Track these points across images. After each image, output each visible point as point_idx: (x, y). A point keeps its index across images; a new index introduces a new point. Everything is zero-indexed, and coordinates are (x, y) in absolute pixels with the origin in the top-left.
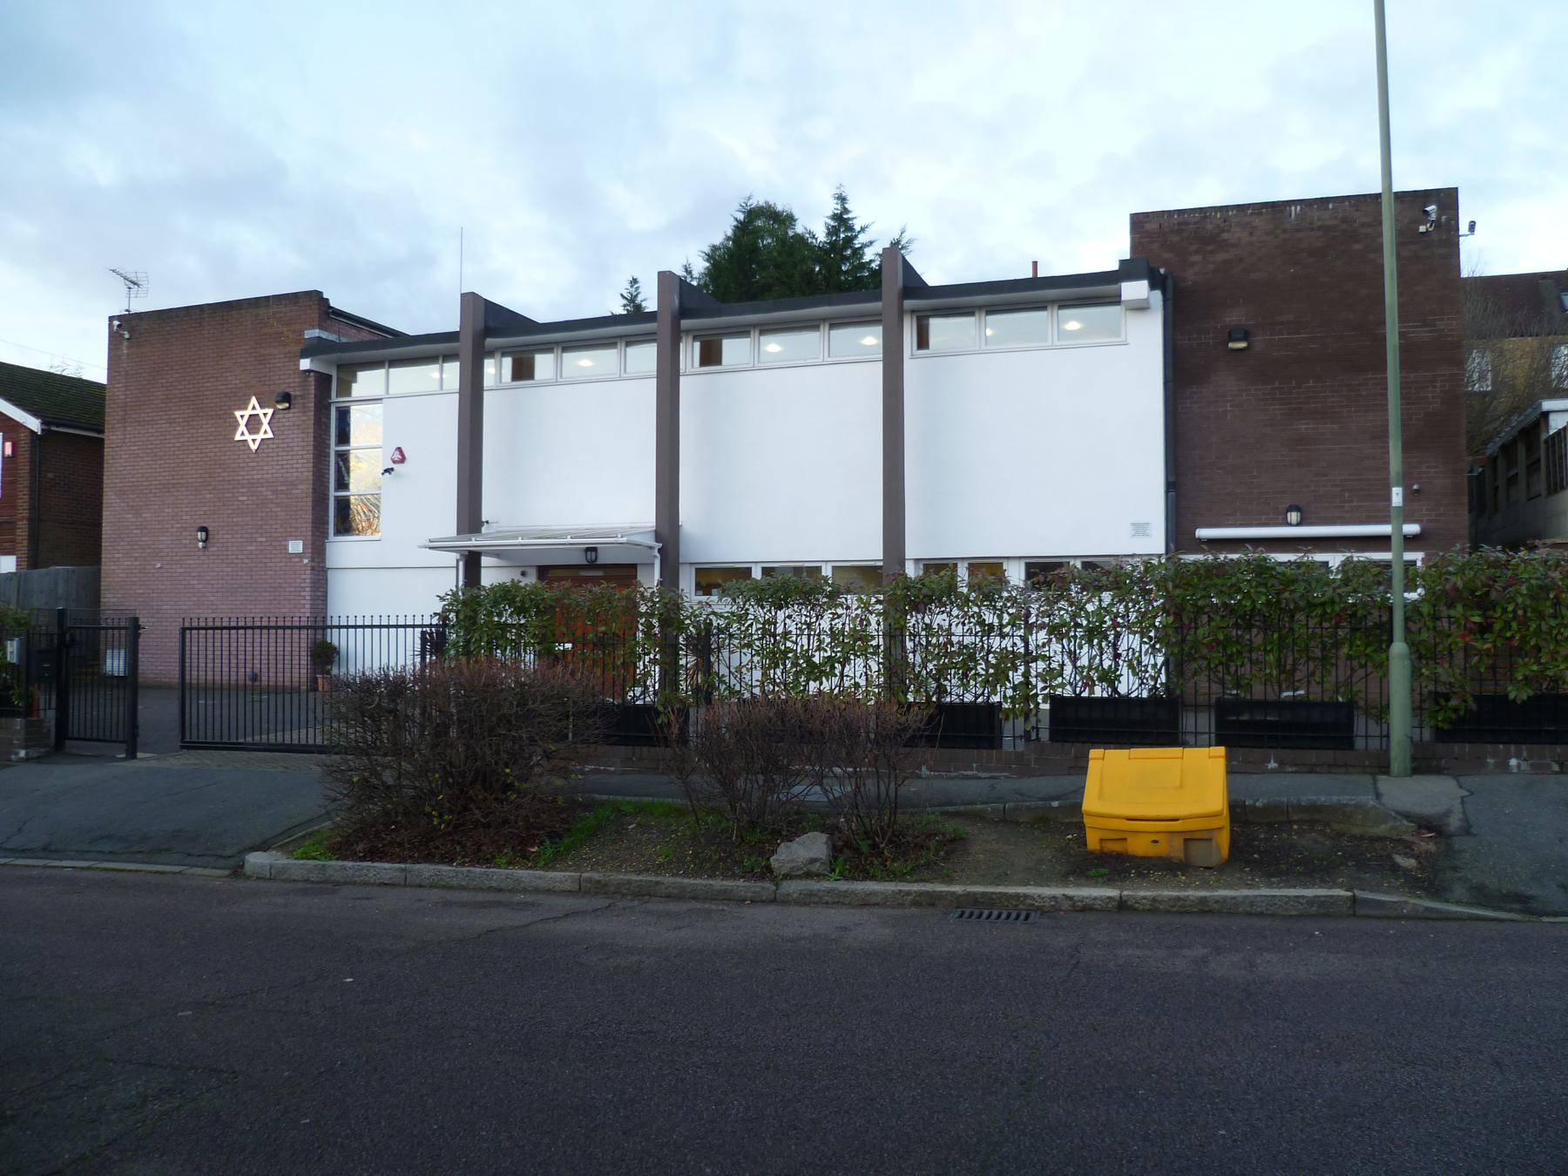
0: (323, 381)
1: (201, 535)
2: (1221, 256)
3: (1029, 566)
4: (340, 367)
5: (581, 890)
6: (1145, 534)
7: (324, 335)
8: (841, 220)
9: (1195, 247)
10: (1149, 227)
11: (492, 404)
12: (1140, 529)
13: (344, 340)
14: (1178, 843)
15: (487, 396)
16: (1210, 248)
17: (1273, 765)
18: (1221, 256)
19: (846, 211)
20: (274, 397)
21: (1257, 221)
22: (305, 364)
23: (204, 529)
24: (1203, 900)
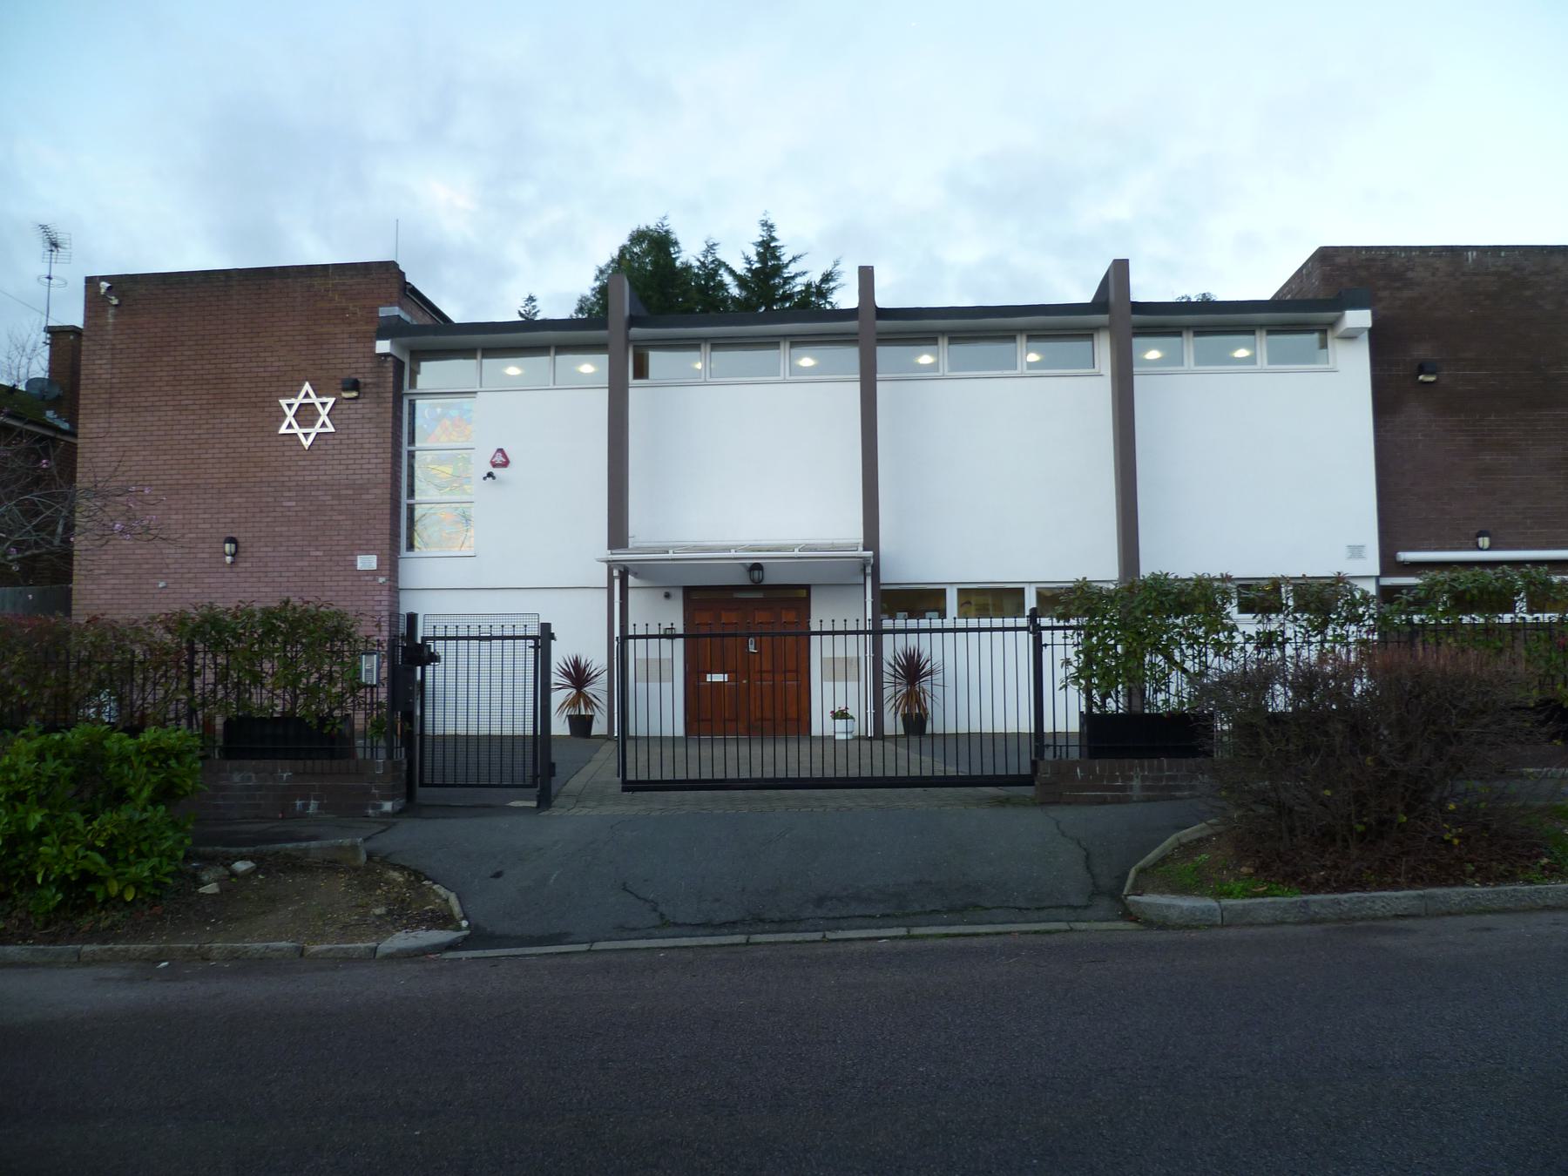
2: (1406, 294)
3: (959, 590)
7: (403, 315)
8: (768, 249)
10: (1339, 260)
12: (1356, 552)
16: (1398, 284)
18: (1406, 294)
20: (344, 382)
22: (383, 346)
23: (232, 540)
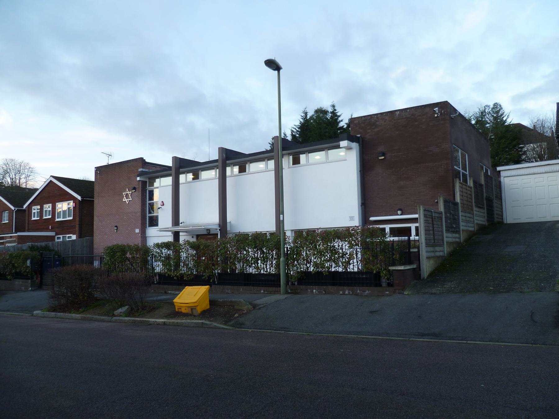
0: (144, 183)
1: (115, 228)
2: (376, 130)
4: (149, 178)
5: (83, 319)
6: (353, 220)
7: (144, 170)
9: (368, 127)
10: (355, 122)
11: (286, 173)
12: (352, 218)
13: (151, 171)
14: (190, 309)
15: (228, 179)
16: (373, 127)
17: (262, 291)
19: (335, 110)
21: (387, 118)
22: (138, 179)
23: (116, 226)
24: (177, 323)
